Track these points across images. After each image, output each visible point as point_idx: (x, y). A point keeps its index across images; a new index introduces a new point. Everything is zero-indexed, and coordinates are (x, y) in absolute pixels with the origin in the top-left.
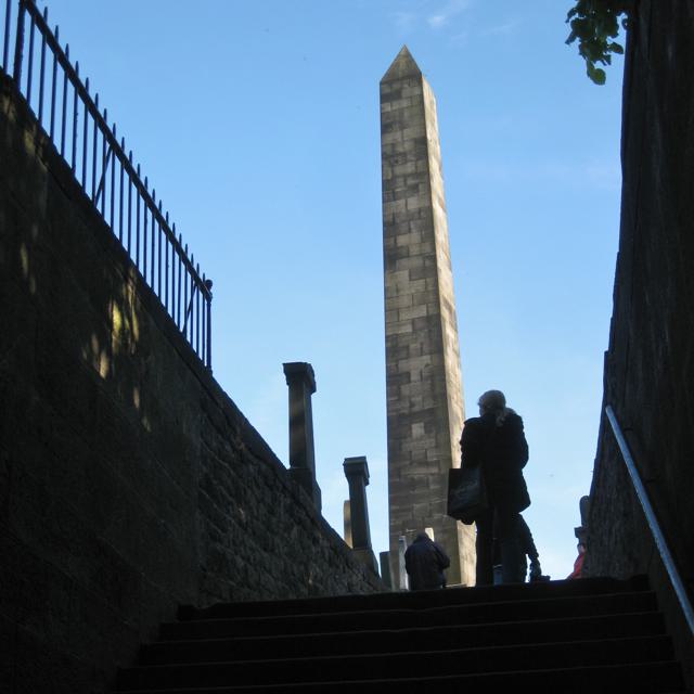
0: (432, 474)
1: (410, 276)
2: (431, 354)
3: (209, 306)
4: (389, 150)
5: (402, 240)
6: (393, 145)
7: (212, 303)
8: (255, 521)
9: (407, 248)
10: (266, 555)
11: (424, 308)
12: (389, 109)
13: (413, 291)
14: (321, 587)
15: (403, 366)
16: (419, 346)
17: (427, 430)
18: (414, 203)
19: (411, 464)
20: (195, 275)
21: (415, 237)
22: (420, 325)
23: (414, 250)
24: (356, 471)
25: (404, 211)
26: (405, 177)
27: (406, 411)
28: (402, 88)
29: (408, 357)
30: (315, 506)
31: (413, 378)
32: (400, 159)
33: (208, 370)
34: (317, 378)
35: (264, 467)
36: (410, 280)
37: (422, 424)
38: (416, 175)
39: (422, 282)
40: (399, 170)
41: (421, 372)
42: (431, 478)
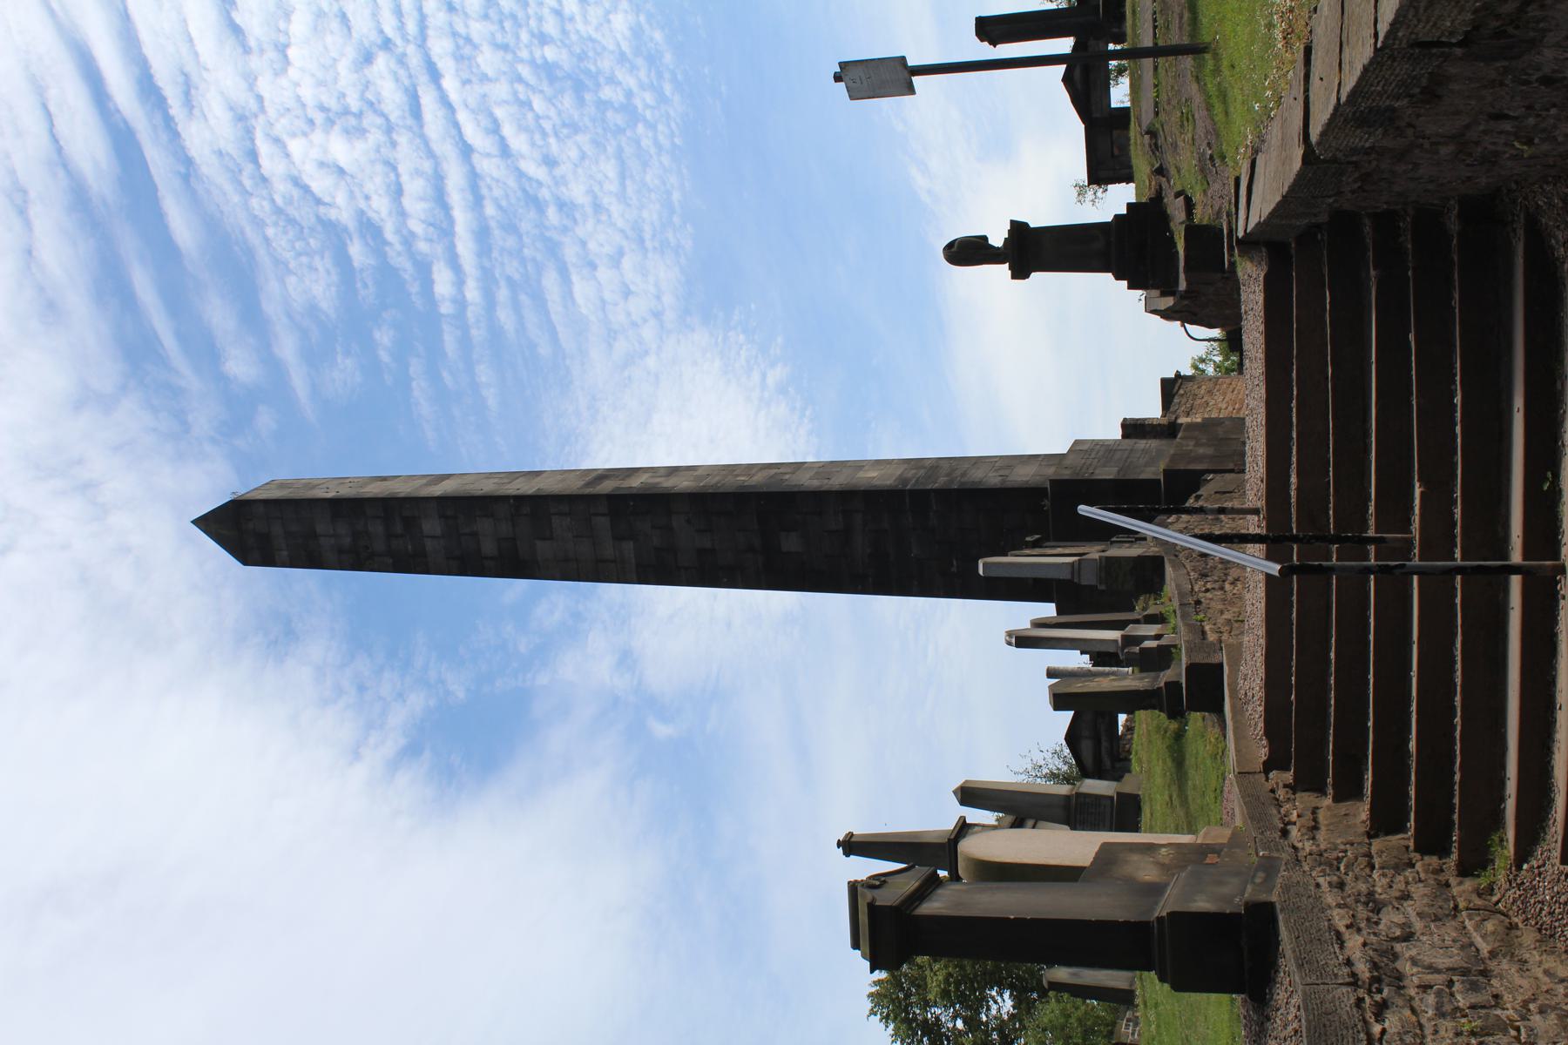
1: (544, 539)
5: (489, 547)
21: (484, 526)
39: (556, 521)
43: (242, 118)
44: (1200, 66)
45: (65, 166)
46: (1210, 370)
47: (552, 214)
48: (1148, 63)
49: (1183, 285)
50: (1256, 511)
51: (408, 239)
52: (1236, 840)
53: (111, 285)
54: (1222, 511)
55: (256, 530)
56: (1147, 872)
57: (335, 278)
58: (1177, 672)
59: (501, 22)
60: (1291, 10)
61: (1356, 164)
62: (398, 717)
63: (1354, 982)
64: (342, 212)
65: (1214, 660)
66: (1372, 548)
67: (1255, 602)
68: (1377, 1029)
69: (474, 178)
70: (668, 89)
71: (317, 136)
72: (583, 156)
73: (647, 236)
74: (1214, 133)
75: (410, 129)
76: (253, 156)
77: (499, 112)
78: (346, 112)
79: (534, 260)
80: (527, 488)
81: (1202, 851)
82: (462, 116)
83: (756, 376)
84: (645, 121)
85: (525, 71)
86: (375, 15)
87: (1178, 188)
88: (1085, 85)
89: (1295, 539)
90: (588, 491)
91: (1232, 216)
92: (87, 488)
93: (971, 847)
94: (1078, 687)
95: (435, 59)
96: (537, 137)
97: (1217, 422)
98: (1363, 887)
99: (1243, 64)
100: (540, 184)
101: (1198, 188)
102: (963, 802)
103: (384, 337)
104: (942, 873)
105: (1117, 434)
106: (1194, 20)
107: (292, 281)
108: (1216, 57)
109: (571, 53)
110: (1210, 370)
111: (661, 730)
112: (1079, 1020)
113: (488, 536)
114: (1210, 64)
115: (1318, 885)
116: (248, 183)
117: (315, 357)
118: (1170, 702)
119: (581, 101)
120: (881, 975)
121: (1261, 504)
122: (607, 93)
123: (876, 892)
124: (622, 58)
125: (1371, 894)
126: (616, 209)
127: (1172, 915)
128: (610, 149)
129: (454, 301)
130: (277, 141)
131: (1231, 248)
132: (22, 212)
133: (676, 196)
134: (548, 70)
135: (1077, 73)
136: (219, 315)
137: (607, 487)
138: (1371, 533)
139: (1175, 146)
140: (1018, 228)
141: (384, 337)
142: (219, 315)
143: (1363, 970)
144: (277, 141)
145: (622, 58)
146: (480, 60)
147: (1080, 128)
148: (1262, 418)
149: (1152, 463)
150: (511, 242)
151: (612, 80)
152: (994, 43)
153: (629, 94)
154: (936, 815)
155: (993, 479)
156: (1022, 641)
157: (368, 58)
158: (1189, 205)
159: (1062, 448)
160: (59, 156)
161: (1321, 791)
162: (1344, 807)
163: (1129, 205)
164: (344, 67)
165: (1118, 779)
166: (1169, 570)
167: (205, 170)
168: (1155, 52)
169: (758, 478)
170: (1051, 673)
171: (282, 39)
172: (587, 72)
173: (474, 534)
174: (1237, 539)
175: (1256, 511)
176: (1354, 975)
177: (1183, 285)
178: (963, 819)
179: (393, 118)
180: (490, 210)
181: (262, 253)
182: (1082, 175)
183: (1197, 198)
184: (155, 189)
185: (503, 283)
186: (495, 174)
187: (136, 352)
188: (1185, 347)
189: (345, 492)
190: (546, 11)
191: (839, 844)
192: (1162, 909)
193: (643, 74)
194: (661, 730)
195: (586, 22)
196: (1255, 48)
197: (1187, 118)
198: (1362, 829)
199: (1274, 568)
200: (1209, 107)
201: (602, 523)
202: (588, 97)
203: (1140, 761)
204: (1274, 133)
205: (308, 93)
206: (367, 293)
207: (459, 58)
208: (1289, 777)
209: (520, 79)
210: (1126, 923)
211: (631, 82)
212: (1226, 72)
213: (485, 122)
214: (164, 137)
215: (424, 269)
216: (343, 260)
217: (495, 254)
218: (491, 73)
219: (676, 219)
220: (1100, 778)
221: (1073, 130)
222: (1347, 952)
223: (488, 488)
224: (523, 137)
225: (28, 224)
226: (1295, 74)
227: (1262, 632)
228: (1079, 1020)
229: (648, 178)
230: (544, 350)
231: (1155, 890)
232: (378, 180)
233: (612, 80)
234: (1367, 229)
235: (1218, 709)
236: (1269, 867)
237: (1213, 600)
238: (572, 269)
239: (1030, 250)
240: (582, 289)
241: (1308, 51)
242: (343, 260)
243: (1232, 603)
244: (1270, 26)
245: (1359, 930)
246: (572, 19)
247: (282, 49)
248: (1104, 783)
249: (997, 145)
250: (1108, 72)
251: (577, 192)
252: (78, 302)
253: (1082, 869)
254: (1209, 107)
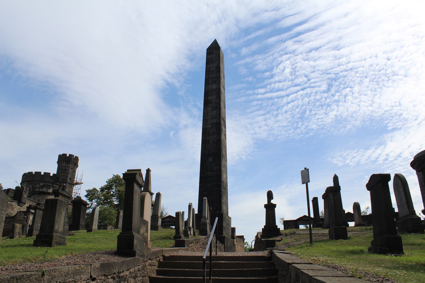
5: (210, 98)
21: (214, 97)
43: (293, 52)
44: (308, 243)
45: (283, 18)
46: (245, 246)
47: (276, 112)
48: (308, 232)
49: (263, 239)
50: (216, 254)
51: (270, 84)
52: (148, 249)
53: (260, 26)
54: (216, 247)
55: (214, 52)
56: (142, 231)
57: (262, 69)
58: (183, 238)
59: (314, 103)
60: (319, 260)
61: (288, 274)
62: (175, 81)
63: (119, 273)
64: (275, 71)
65: (186, 246)
66: (209, 278)
67: (198, 254)
68: (109, 277)
69: (282, 97)
70: (301, 136)
71: (290, 66)
72: (287, 119)
73: (272, 131)
74: (294, 246)
75: (292, 84)
76: (286, 54)
77: (296, 102)
78: (295, 72)
79: (266, 109)
80: (222, 106)
81: (146, 242)
82: (295, 95)
83: (243, 153)
84: (295, 131)
85: (304, 107)
86: (314, 78)
87: (283, 239)
88: (303, 220)
89: (211, 262)
90: (221, 118)
91: (277, 249)
92: (220, 21)
93: (148, 195)
94: (180, 218)
95: (306, 89)
96: (291, 110)
97: (235, 247)
98: (139, 275)
99: (308, 251)
100: (282, 110)
101: (283, 243)
102: (157, 194)
103: (250, 79)
104: (143, 188)
105: (232, 226)
106: (317, 242)
107: (261, 61)
108: (310, 246)
109: (308, 117)
110: (245, 246)
111: (172, 133)
112: (112, 218)
113: (212, 98)
114: (308, 245)
115: (139, 266)
116: (281, 53)
117: (246, 65)
118: (177, 237)
119: (298, 118)
120: (122, 176)
121: (218, 255)
122: (300, 124)
123: (139, 175)
124: (307, 127)
125: (137, 277)
126: (277, 125)
127: (133, 236)
128: (289, 124)
129: (258, 93)
130: (289, 59)
131: (270, 249)
132: (274, 10)
133: (280, 137)
134: (304, 112)
135: (306, 218)
136: (255, 47)
137: (222, 122)
138: (212, 278)
139: (291, 238)
140: (275, 206)
141: (250, 79)
142: (255, 47)
143: (122, 274)
144: (289, 59)
145: (307, 127)
146: (306, 98)
147: (295, 218)
148: (236, 255)
149: (226, 234)
150: (270, 104)
151: (303, 125)
152: (312, 201)
153: (300, 128)
154: (154, 188)
155: (223, 201)
156: (190, 206)
157: (306, 76)
158: (279, 241)
159: (230, 215)
160: (285, 17)
161: (158, 267)
162: (155, 272)
163: (279, 229)
164: (304, 71)
165: (161, 226)
166: (204, 237)
167: (283, 44)
168: (311, 234)
169: (224, 153)
170: (183, 212)
171: (309, 60)
172: (304, 120)
174: (211, 251)
175: (216, 254)
176: (121, 273)
177: (263, 239)
178: (153, 194)
179: (294, 81)
180: (276, 100)
181: (267, 55)
182: (285, 219)
183: (281, 242)
184: (279, 35)
185: (261, 102)
186: (284, 101)
187: (247, 31)
188: (250, 241)
189: (221, 69)
190: (316, 111)
191: (149, 169)
192: (135, 234)
193: (304, 131)
194: (172, 133)
195: (314, 120)
196: (311, 254)
197: (297, 240)
198: (150, 275)
199: (205, 257)
200: (299, 245)
201: (215, 121)
202: (299, 120)
203: (165, 230)
204: (294, 257)
205: (299, 64)
206: (259, 76)
207: (306, 94)
208: (161, 260)
209: (302, 106)
210: (132, 226)
211: (302, 128)
212: (307, 248)
213: (294, 99)
214: (289, 37)
215: (264, 87)
216: (266, 71)
217: (267, 101)
218: (303, 100)
219: (275, 137)
220: (162, 222)
221: (295, 218)
222: (125, 271)
223: (222, 98)
224: (291, 107)
225: (272, 11)
226: (306, 261)
227: (191, 255)
228: (112, 218)
229: (283, 132)
230: (248, 111)
231: (138, 232)
232: (282, 78)
233: (303, 125)
234: (274, 277)
235: (175, 246)
236: (143, 256)
237: (198, 246)
238: (264, 116)
239: (270, 208)
240: (261, 118)
241: (311, 264)
242: (266, 71)
243: (197, 249)
244: (316, 256)
245: (130, 274)
246: (315, 117)
247: (307, 60)
248: (160, 223)
249: (291, 203)
250: (306, 225)
251: (280, 117)
252: (257, 20)
253: (143, 217)
254: (299, 245)
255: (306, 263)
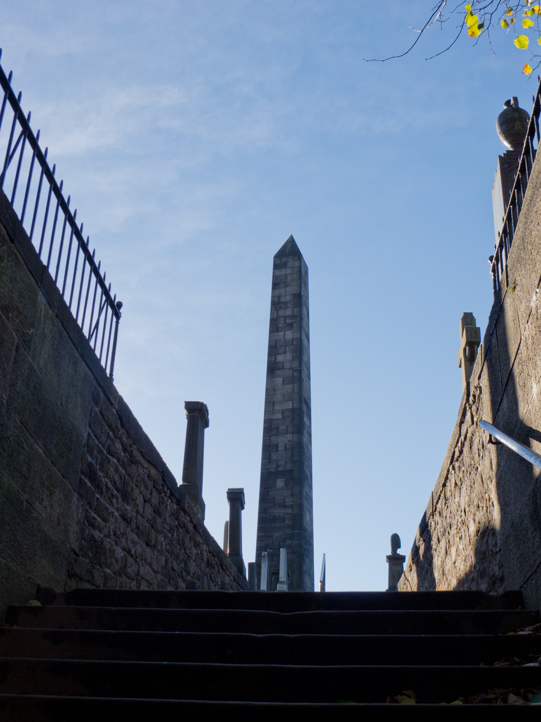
0: (287, 514)
1: (283, 381)
2: (293, 433)
3: (117, 323)
4: (276, 300)
5: (280, 358)
6: (279, 297)
7: (120, 321)
8: (140, 518)
9: (283, 363)
10: (148, 550)
11: (290, 404)
12: (278, 273)
13: (285, 392)
14: (198, 584)
15: (274, 439)
16: (285, 428)
17: (287, 485)
18: (289, 335)
19: (274, 506)
20: (106, 292)
21: (289, 356)
22: (287, 414)
23: (287, 365)
24: (236, 498)
25: (282, 339)
26: (285, 317)
27: (274, 470)
28: (287, 262)
29: (277, 434)
30: (199, 516)
31: (279, 449)
32: (282, 305)
33: (111, 378)
34: (211, 417)
35: (153, 472)
36: (283, 384)
37: (283, 480)
38: (292, 317)
39: (290, 386)
40: (281, 313)
41: (286, 445)
42: (286, 516)
113: (284, 358)
173: (285, 352)
255: (518, 349)
